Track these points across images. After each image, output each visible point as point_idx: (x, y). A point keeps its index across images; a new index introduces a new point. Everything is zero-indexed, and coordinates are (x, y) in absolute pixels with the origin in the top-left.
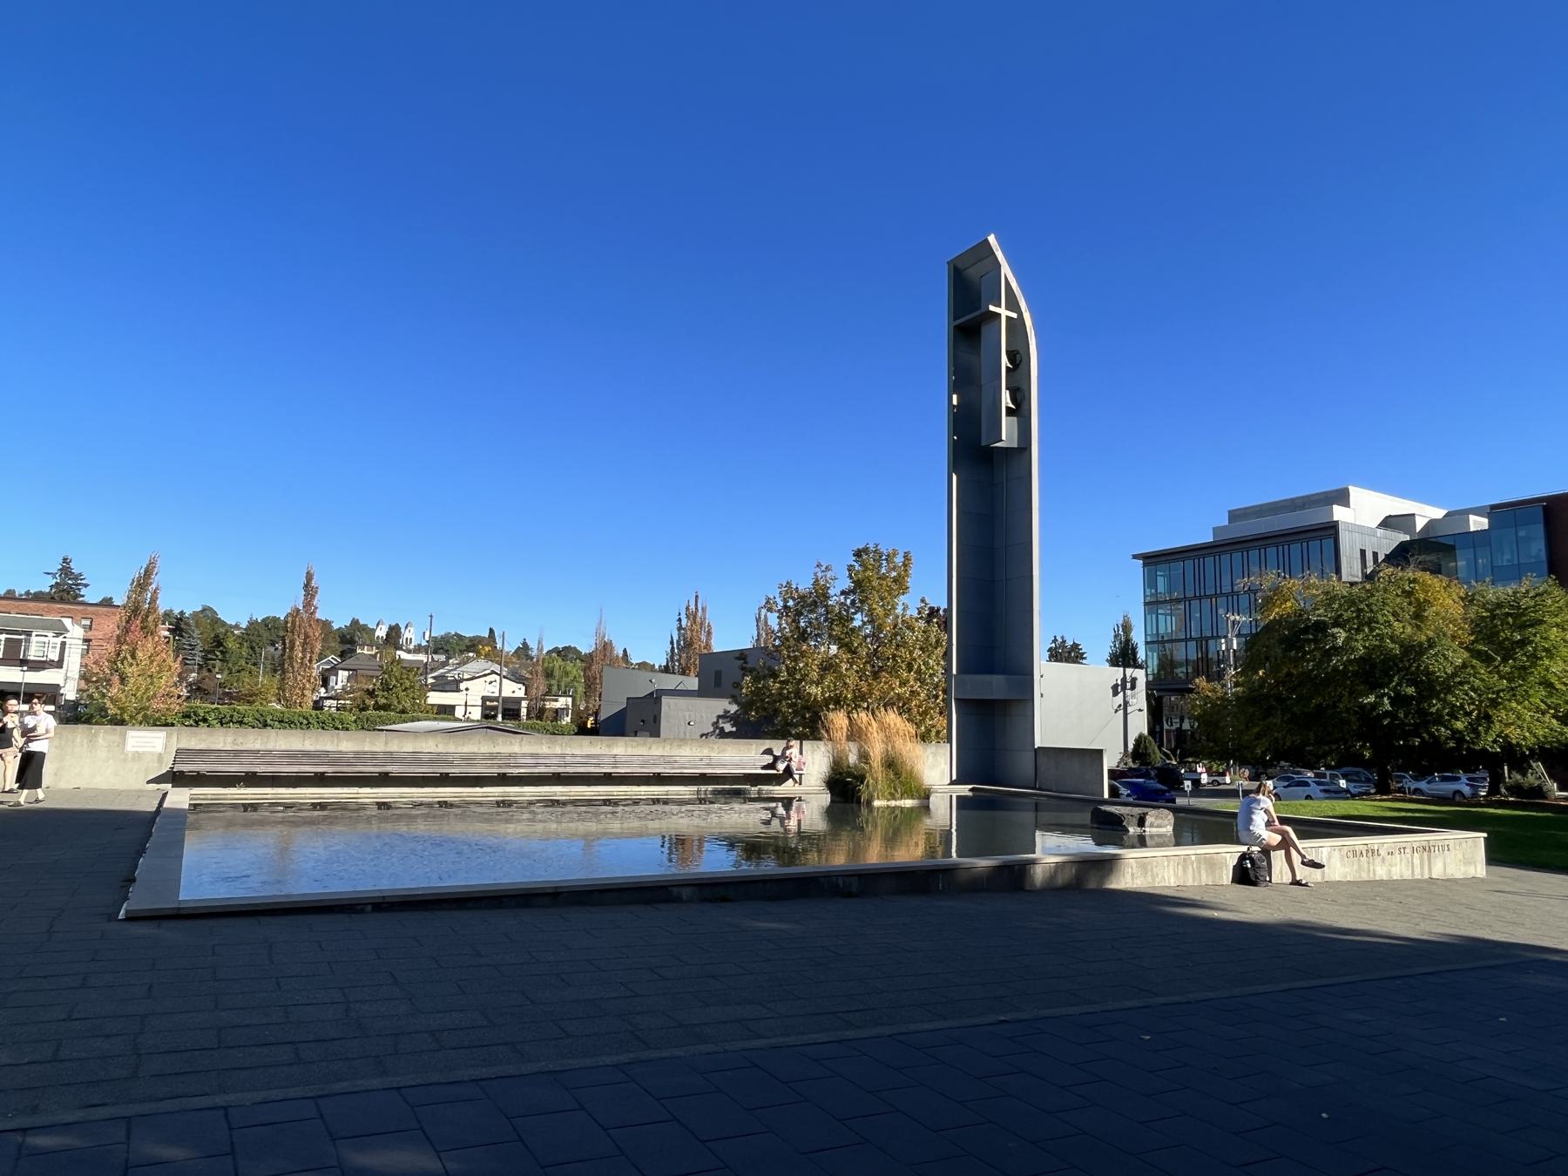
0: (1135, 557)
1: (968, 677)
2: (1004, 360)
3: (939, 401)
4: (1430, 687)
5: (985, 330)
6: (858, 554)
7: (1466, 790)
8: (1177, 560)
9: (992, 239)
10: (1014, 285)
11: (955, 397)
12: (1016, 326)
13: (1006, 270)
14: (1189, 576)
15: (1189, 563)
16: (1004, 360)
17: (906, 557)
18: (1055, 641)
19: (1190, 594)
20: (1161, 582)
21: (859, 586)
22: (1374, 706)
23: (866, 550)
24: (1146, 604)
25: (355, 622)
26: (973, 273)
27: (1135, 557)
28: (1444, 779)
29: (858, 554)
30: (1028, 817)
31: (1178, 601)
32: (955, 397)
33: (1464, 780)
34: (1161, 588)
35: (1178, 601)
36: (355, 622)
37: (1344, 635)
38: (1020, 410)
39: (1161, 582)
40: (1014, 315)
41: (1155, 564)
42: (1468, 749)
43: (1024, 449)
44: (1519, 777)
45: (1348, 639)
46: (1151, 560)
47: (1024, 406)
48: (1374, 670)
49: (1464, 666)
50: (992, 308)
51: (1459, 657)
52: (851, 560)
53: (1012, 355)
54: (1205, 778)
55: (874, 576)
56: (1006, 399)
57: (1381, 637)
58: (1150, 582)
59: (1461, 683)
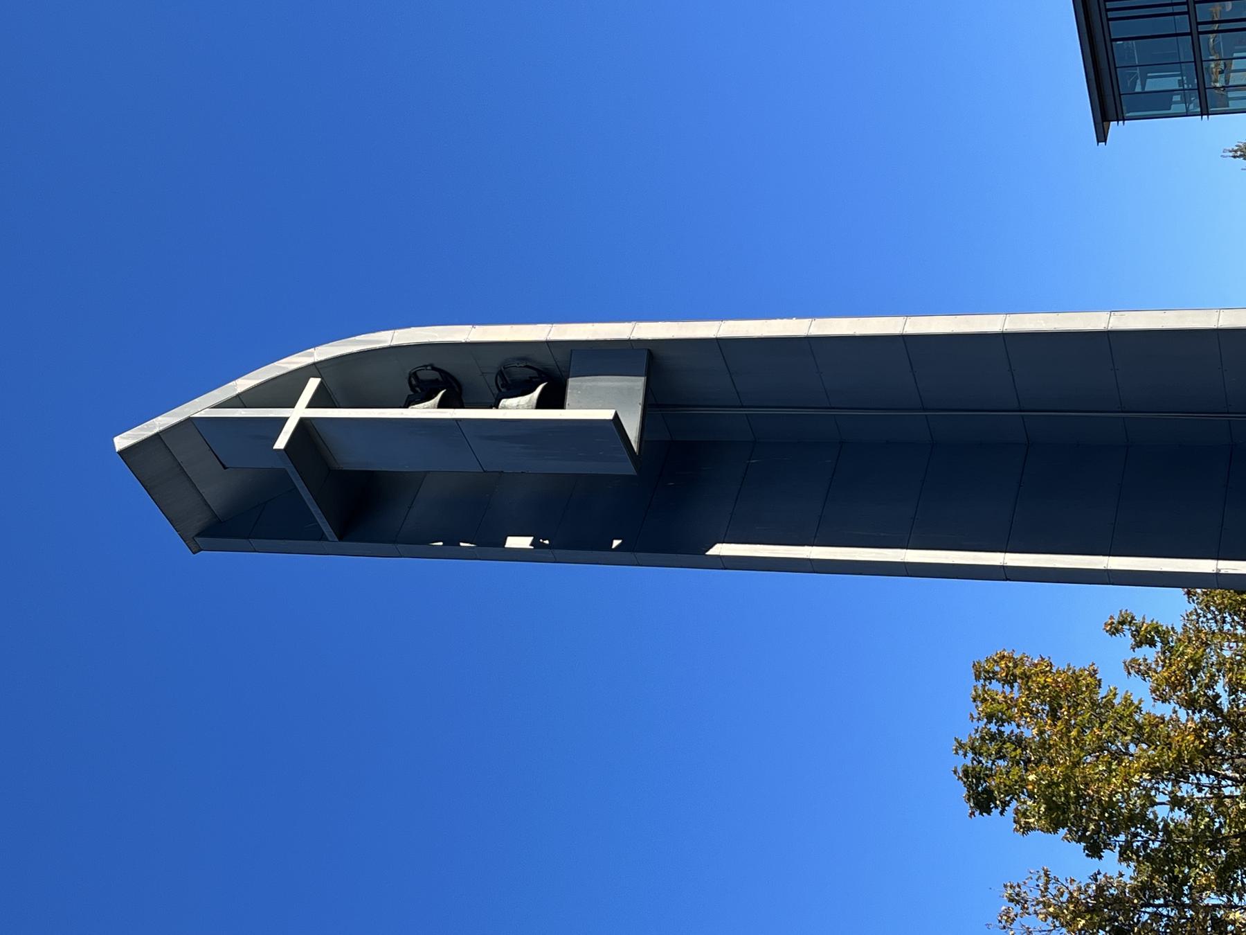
0: (1102, 136)
2: (426, 411)
3: (524, 590)
5: (352, 458)
6: (983, 802)
8: (1110, 52)
9: (122, 442)
10: (243, 384)
11: (513, 542)
12: (340, 382)
13: (201, 407)
14: (1144, 27)
15: (1117, 29)
16: (426, 411)
17: (983, 674)
19: (1183, 24)
20: (1155, 84)
21: (1064, 811)
23: (973, 777)
24: (1205, 111)
26: (217, 490)
27: (1102, 136)
29: (983, 802)
31: (1196, 48)
32: (513, 542)
34: (1171, 83)
35: (1196, 48)
38: (548, 373)
39: (1155, 84)
40: (313, 384)
41: (1117, 96)
43: (649, 360)
46: (1109, 105)
47: (547, 360)
50: (281, 443)
52: (1000, 822)
53: (420, 394)
55: (1037, 758)
56: (519, 408)
58: (1157, 106)
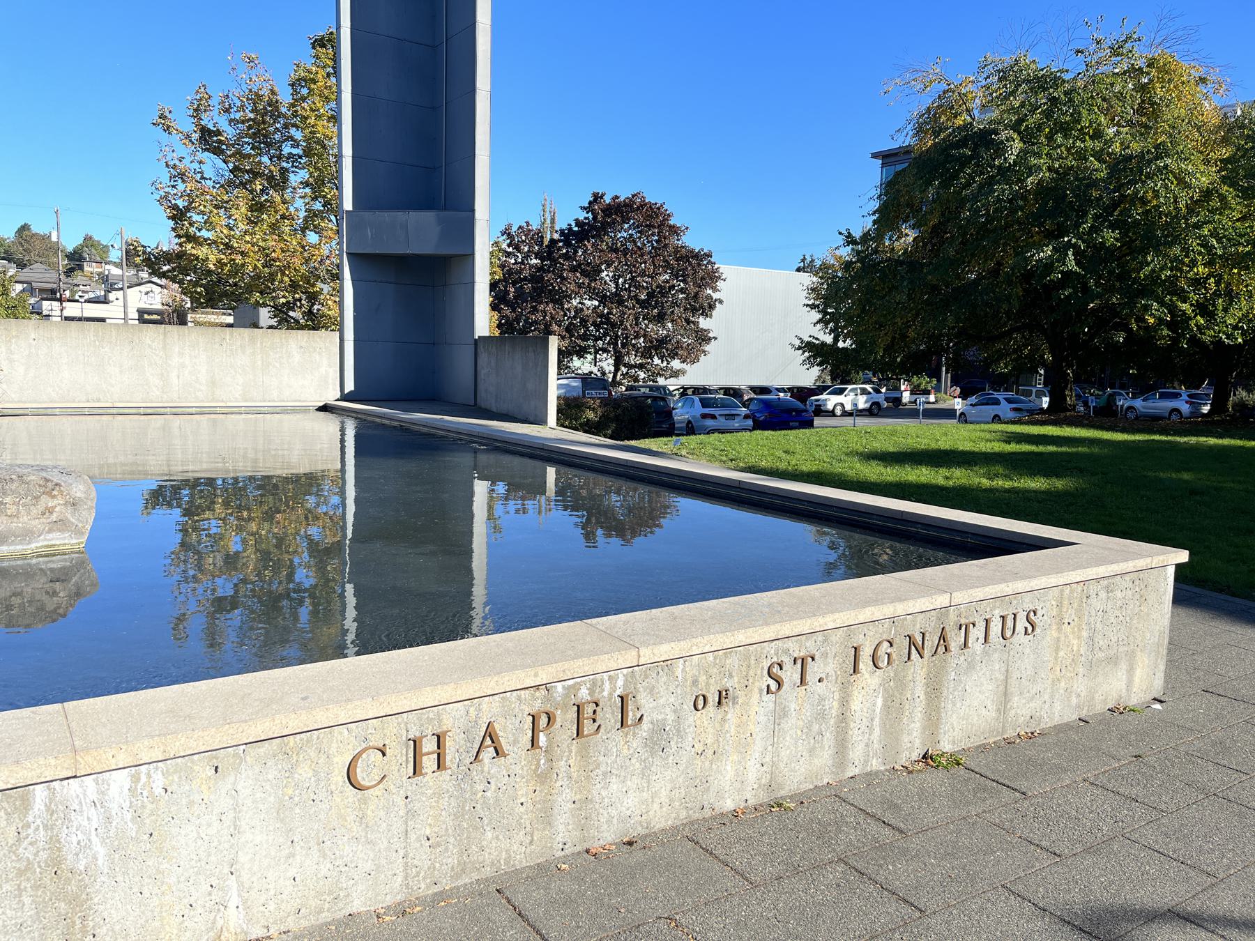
1: (367, 215)
4: (1149, 234)
7: (1185, 408)
18: (803, 260)
22: (1048, 266)
25: (88, 239)
27: (874, 156)
28: (1164, 396)
30: (465, 459)
33: (1184, 397)
36: (88, 239)
37: (1018, 144)
42: (1194, 341)
44: (1244, 394)
45: (1023, 154)
48: (1060, 204)
49: (1207, 194)
51: (1204, 178)
54: (906, 397)
57: (1081, 156)
59: (1198, 226)
